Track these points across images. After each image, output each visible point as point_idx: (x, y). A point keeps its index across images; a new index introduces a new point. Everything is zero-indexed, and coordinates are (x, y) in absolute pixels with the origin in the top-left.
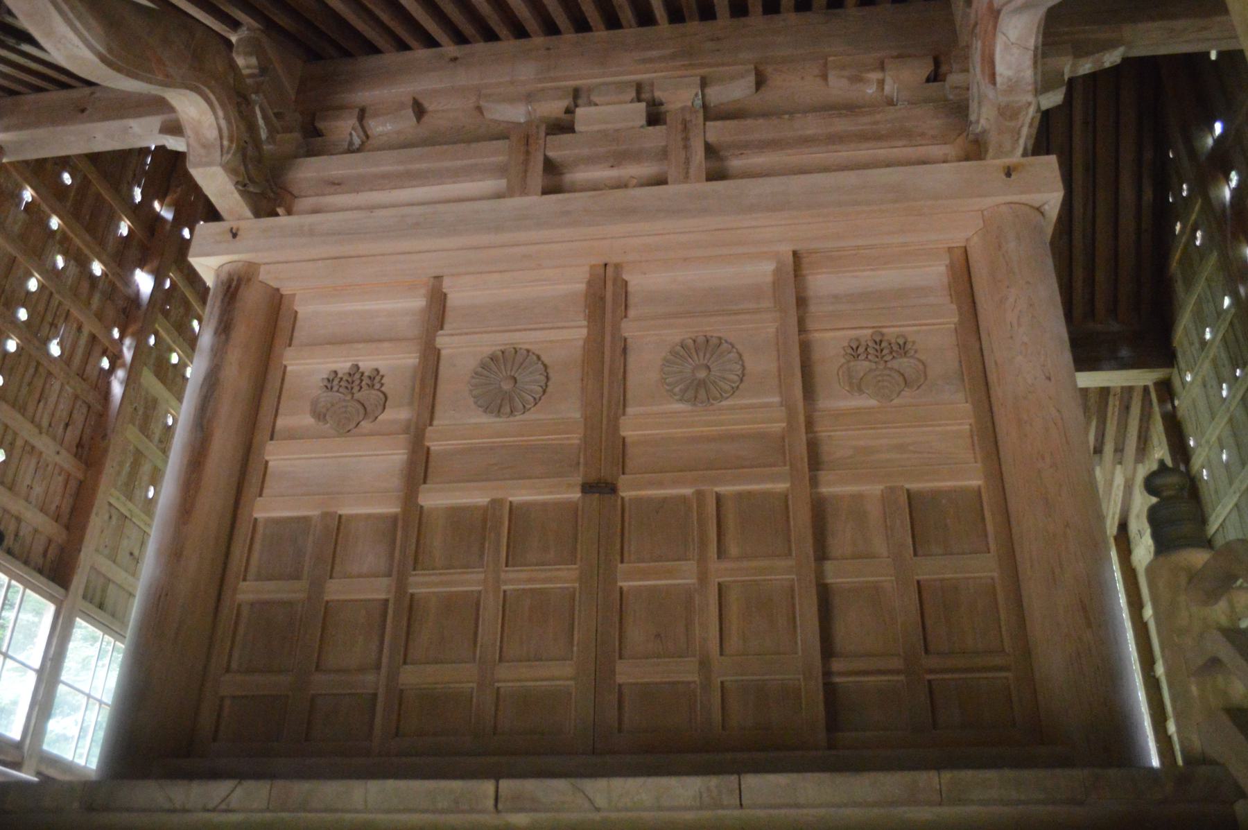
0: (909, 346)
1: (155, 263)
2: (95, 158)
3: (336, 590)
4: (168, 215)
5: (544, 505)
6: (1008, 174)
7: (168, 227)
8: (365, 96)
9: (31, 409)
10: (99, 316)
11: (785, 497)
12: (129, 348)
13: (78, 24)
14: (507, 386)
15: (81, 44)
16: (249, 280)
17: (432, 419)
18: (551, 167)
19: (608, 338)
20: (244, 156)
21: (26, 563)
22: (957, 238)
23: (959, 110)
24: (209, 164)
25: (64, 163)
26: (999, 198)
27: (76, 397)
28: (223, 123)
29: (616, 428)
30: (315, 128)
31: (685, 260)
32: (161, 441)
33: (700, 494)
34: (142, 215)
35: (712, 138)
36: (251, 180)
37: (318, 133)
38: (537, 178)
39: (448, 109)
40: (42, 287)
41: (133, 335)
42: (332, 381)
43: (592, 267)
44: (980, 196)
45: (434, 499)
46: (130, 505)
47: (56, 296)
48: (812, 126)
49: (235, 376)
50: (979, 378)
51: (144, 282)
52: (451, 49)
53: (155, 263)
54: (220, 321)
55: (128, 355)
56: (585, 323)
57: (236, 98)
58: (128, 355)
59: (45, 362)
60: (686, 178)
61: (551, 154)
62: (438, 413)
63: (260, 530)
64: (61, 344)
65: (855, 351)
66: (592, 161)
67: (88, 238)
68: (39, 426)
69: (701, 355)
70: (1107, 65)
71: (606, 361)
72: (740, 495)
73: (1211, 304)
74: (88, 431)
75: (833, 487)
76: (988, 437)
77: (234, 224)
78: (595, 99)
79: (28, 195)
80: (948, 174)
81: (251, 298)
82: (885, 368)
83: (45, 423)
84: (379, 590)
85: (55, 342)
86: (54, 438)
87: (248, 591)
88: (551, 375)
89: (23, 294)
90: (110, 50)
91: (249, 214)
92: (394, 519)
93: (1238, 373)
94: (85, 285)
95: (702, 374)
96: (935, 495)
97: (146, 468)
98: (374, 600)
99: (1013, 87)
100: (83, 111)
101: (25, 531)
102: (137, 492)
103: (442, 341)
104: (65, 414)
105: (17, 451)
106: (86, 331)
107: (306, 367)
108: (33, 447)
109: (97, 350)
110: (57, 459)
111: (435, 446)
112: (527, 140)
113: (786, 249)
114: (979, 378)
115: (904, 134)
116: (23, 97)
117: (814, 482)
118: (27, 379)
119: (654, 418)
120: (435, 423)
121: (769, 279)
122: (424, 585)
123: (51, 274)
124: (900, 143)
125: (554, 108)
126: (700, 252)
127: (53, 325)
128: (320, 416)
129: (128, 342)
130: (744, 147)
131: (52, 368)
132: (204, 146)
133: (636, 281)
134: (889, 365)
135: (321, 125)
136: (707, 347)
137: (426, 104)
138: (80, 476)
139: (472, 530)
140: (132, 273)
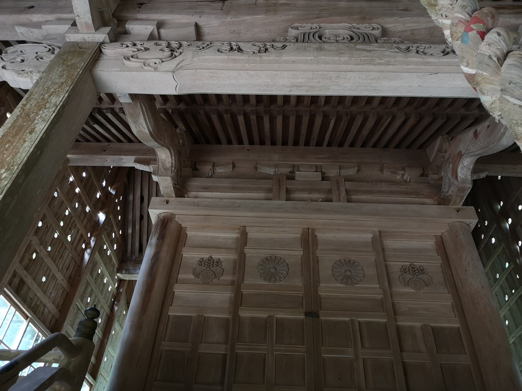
0: (424, 271)
1: (107, 210)
2: (94, 168)
3: (203, 349)
4: (113, 193)
5: (290, 320)
6: (458, 212)
7: (113, 197)
8: (214, 159)
9: (57, 262)
10: (85, 228)
11: (385, 325)
12: (93, 241)
13: (147, 120)
14: (273, 271)
15: (146, 127)
16: (172, 220)
17: (243, 281)
18: (288, 191)
19: (311, 256)
20: (178, 174)
21: (44, 324)
22: (439, 233)
23: (437, 187)
24: (166, 176)
25: (84, 168)
26: (455, 220)
27: (72, 258)
28: (173, 161)
29: (316, 291)
30: (196, 167)
31: (338, 230)
32: (95, 279)
33: (352, 321)
34: (104, 191)
35: (348, 187)
36: (178, 184)
37: (196, 169)
38: (283, 195)
39: (244, 168)
40: (70, 213)
41: (95, 236)
42: (201, 262)
43: (303, 229)
44: (448, 218)
45: (245, 314)
46: (81, 304)
47: (74, 218)
48: (384, 187)
49: (165, 256)
50: (454, 286)
51: (102, 217)
52: (246, 145)
53: (107, 210)
54: (160, 235)
55: (92, 244)
56: (302, 249)
57: (178, 154)
58: (92, 244)
59: (65, 243)
60: (339, 201)
61: (288, 187)
62: (245, 279)
63: (171, 320)
64: (71, 237)
65: (404, 270)
66: (302, 190)
67: (87, 197)
68: (58, 269)
69: (347, 266)
70: (481, 177)
71: (310, 265)
72: (252, 319)
73: (500, 265)
74: (74, 272)
75: (404, 322)
76: (460, 307)
77: (168, 199)
78: (301, 169)
79: (71, 179)
80: (435, 209)
81: (172, 227)
82: (417, 278)
83: (61, 267)
84: (221, 350)
85: (69, 236)
86: (62, 274)
87: (166, 345)
88: (290, 268)
89: (63, 216)
90: (153, 131)
91: (174, 196)
92: (227, 320)
93: (513, 291)
94: (83, 215)
95: (349, 273)
96: (442, 329)
97: (89, 290)
98: (219, 354)
99: (464, 181)
100: (105, 151)
101: (46, 311)
102: (85, 299)
103: (246, 250)
104: (68, 264)
105: (50, 278)
106: (80, 232)
107: (190, 255)
108: (55, 277)
109: (82, 241)
110: (62, 283)
111: (245, 291)
112: (279, 181)
113: (376, 230)
114: (454, 286)
115: (417, 194)
116: (81, 143)
117: (396, 321)
118: (58, 249)
119: (330, 289)
120: (244, 282)
121: (370, 240)
122: (241, 349)
123: (73, 208)
124: (414, 196)
125: (286, 170)
126: (344, 228)
127: (70, 229)
128: (197, 275)
129: (93, 238)
130: (357, 192)
131: (67, 246)
132: (165, 169)
133: (320, 236)
134: (418, 277)
135: (198, 167)
136: (350, 263)
137: (236, 164)
138: (68, 291)
139: (261, 328)
140: (99, 213)
